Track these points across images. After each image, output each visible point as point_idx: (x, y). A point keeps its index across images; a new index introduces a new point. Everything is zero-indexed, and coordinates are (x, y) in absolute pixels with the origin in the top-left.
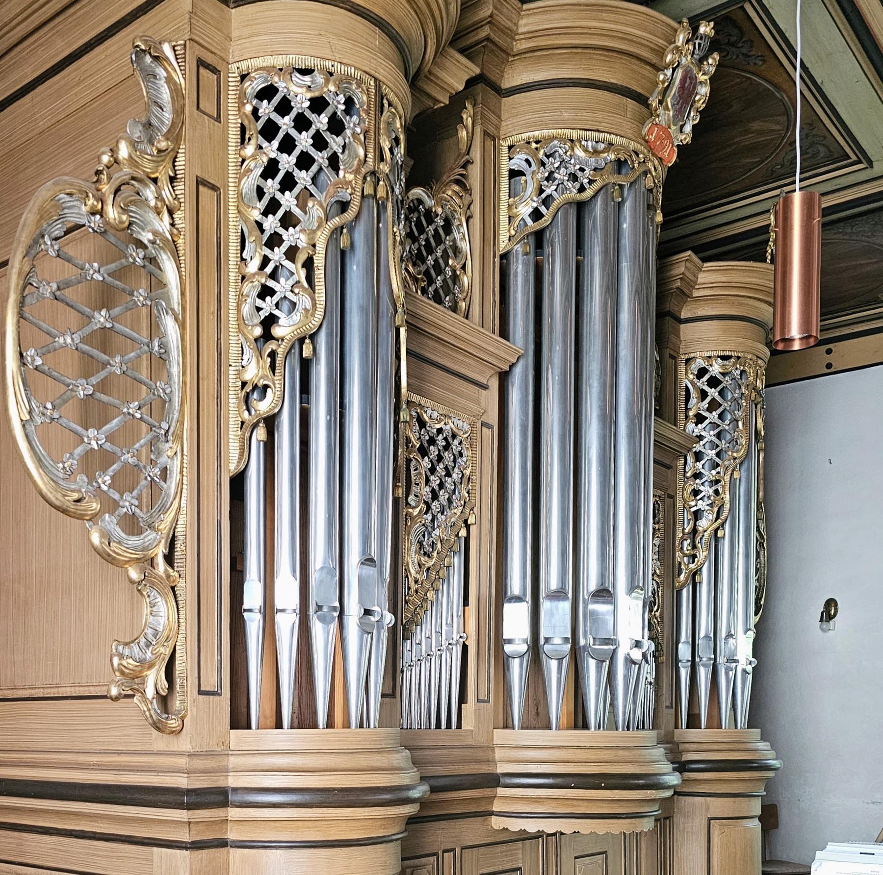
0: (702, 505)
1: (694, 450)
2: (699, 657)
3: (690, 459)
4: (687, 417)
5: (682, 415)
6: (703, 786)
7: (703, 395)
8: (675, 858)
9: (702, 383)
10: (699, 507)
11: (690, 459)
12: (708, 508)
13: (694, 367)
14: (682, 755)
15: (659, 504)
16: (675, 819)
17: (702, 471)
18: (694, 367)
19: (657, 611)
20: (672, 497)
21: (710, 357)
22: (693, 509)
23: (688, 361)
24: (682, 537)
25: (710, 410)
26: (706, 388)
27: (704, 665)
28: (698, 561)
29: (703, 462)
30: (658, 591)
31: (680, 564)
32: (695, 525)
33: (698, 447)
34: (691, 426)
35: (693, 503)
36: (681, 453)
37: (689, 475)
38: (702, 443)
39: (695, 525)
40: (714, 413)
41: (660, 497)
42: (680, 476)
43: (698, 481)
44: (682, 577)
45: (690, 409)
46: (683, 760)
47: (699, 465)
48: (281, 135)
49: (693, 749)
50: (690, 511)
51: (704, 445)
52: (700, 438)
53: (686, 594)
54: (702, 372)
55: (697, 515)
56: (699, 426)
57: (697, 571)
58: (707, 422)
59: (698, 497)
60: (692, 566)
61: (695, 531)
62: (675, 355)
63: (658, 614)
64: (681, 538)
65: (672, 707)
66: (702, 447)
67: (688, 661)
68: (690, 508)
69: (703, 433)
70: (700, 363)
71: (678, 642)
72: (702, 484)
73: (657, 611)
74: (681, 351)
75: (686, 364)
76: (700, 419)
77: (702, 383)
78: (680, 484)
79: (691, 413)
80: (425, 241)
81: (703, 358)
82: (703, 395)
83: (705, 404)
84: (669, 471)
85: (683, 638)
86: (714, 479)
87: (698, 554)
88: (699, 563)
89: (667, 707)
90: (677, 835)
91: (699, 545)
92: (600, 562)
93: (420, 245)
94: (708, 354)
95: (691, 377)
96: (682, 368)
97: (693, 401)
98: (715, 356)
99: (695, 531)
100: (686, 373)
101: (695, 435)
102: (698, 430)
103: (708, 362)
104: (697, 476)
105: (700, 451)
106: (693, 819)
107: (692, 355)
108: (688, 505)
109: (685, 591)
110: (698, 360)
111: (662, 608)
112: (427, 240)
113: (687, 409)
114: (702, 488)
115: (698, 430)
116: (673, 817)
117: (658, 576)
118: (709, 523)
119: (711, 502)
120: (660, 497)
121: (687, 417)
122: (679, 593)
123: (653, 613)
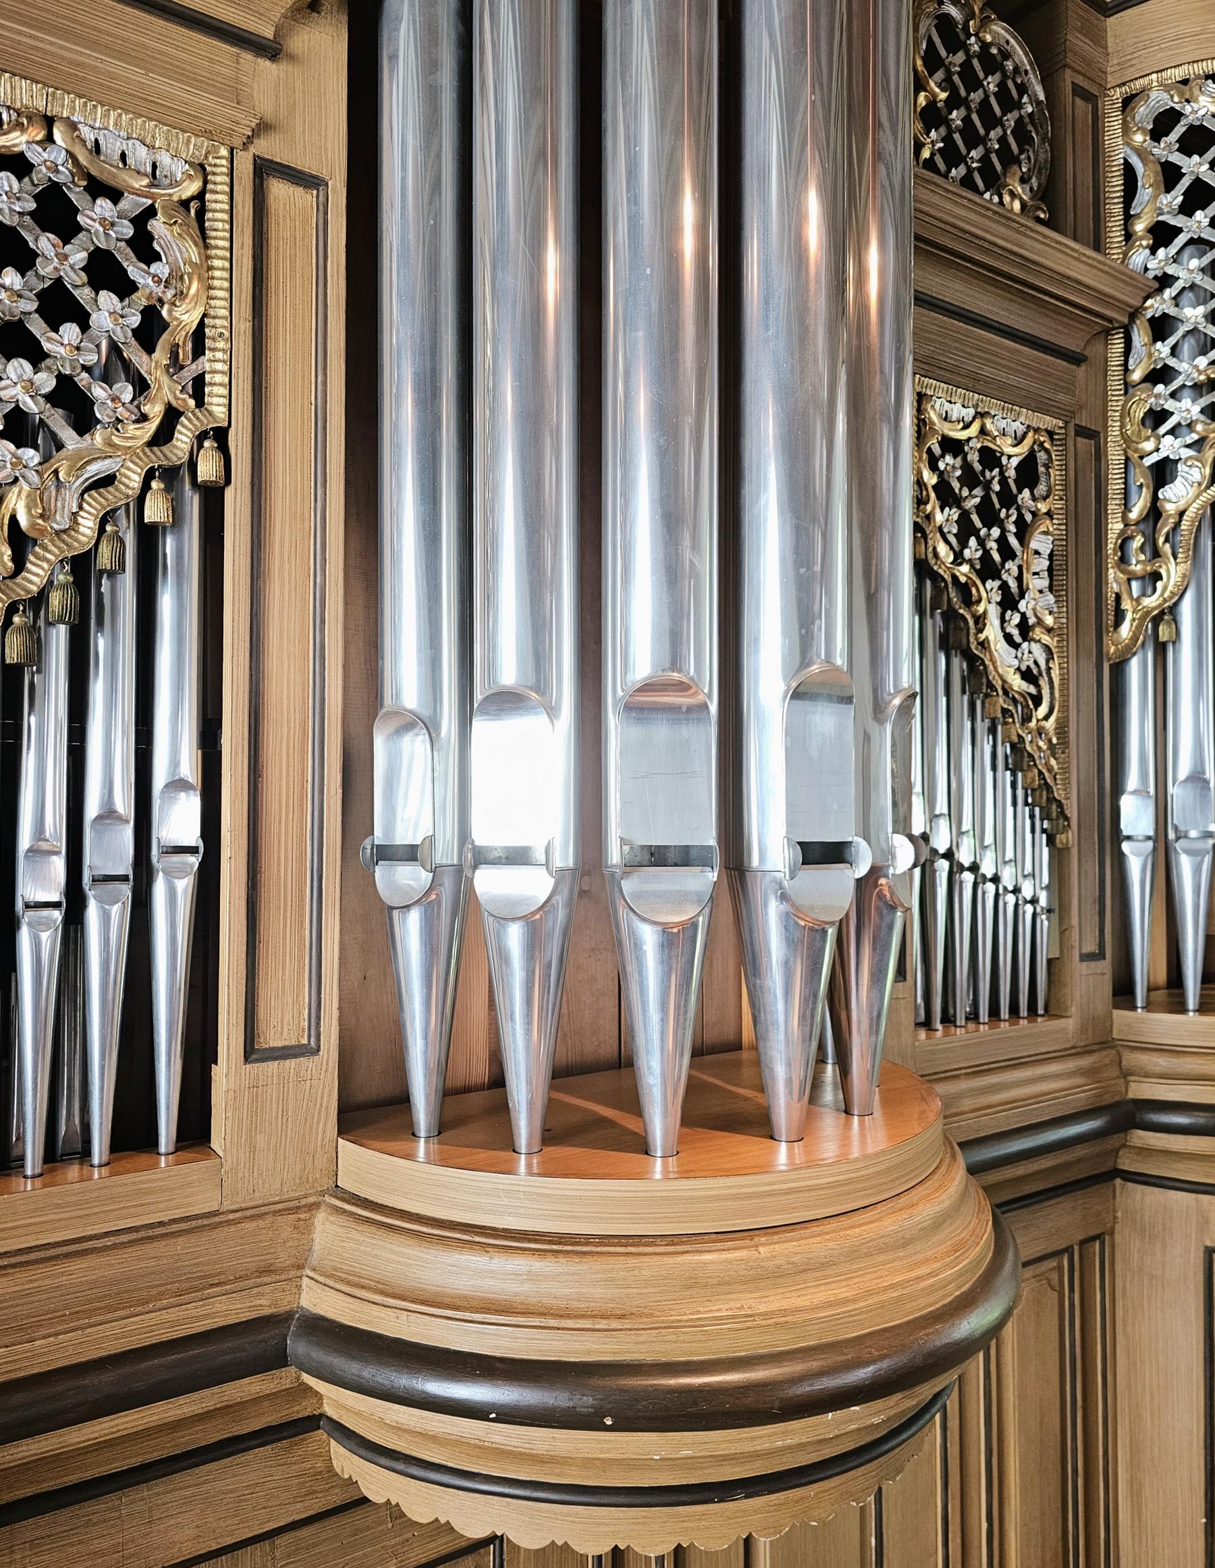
0: (1170, 447)
1: (1149, 314)
2: (1176, 828)
3: (1140, 336)
4: (1128, 236)
5: (1115, 235)
6: (1180, 1166)
7: (1171, 175)
8: (1119, 1337)
9: (1167, 149)
10: (1162, 454)
11: (1140, 336)
12: (1190, 452)
13: (1144, 113)
14: (1127, 1083)
15: (1047, 451)
16: (1118, 1238)
17: (1172, 362)
18: (1144, 113)
19: (1046, 718)
20: (1093, 435)
21: (1185, 82)
22: (1148, 461)
23: (1128, 102)
24: (1122, 532)
25: (1187, 209)
26: (1177, 158)
27: (1189, 852)
28: (1165, 588)
29: (1171, 341)
30: (1049, 669)
31: (1118, 597)
32: (1155, 498)
33: (1157, 305)
34: (1139, 257)
35: (1148, 446)
36: (1110, 320)
37: (1136, 376)
38: (1168, 293)
39: (1155, 498)
40: (1199, 214)
41: (1051, 434)
42: (1115, 383)
43: (1160, 388)
44: (1125, 630)
45: (1138, 216)
46: (1131, 1095)
47: (1163, 349)
48: (1185, 183)
49: (1158, 1070)
50: (1141, 466)
51: (1175, 298)
52: (1165, 281)
53: (1137, 672)
54: (1165, 122)
55: (1163, 472)
56: (1161, 252)
57: (1162, 613)
58: (1181, 240)
59: (1163, 430)
60: (1151, 602)
61: (1155, 513)
62: (1094, 90)
63: (1050, 724)
64: (1120, 535)
65: (1100, 956)
66: (1170, 303)
67: (1149, 838)
68: (1141, 458)
69: (1171, 270)
70: (1159, 100)
71: (1118, 789)
72: (1173, 395)
73: (1046, 718)
74: (1111, 81)
75: (1123, 111)
76: (1162, 234)
77: (1167, 149)
78: (1116, 403)
79: (1140, 227)
80: (999, 141)
81: (1167, 88)
82: (1171, 175)
83: (1176, 197)
84: (1081, 371)
85: (1132, 780)
86: (1202, 377)
87: (1163, 572)
88: (1167, 594)
89: (1087, 957)
90: (1126, 1282)
91: (1167, 547)
92: (426, 611)
93: (988, 151)
94: (1178, 74)
95: (1139, 138)
96: (1114, 123)
97: (1144, 193)
98: (1198, 77)
99: (1155, 513)
100: (1126, 130)
101: (1151, 274)
102: (1160, 261)
103: (1181, 94)
104: (1160, 375)
105: (1165, 315)
106: (1164, 1246)
107: (1139, 84)
108: (1136, 450)
109: (1134, 665)
110: (1154, 95)
111: (1065, 708)
112: (1002, 140)
113: (1128, 218)
114: (1170, 405)
115: (1160, 261)
116: (1112, 1233)
117: (1049, 630)
118: (1192, 492)
119: (1195, 437)
120: (1051, 434)
121: (1128, 236)
122: (1119, 670)
123: (1033, 724)
